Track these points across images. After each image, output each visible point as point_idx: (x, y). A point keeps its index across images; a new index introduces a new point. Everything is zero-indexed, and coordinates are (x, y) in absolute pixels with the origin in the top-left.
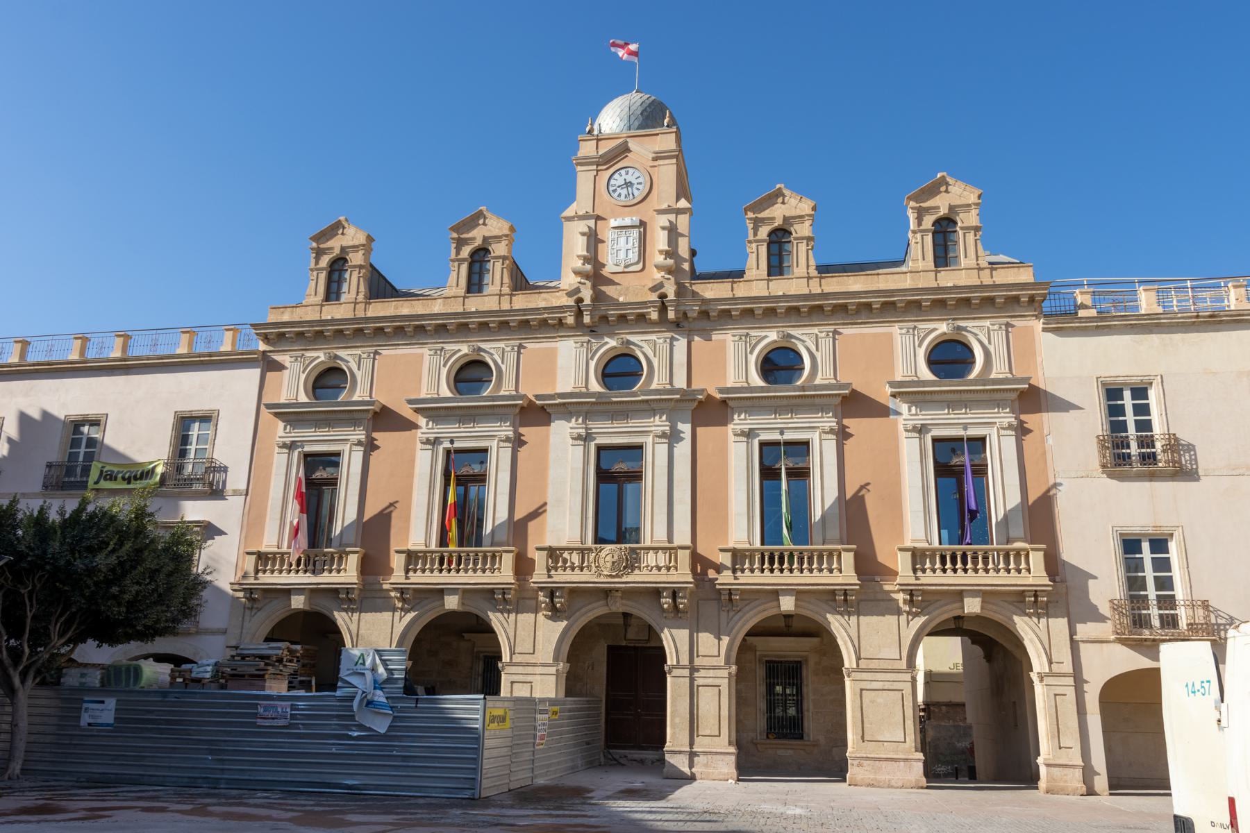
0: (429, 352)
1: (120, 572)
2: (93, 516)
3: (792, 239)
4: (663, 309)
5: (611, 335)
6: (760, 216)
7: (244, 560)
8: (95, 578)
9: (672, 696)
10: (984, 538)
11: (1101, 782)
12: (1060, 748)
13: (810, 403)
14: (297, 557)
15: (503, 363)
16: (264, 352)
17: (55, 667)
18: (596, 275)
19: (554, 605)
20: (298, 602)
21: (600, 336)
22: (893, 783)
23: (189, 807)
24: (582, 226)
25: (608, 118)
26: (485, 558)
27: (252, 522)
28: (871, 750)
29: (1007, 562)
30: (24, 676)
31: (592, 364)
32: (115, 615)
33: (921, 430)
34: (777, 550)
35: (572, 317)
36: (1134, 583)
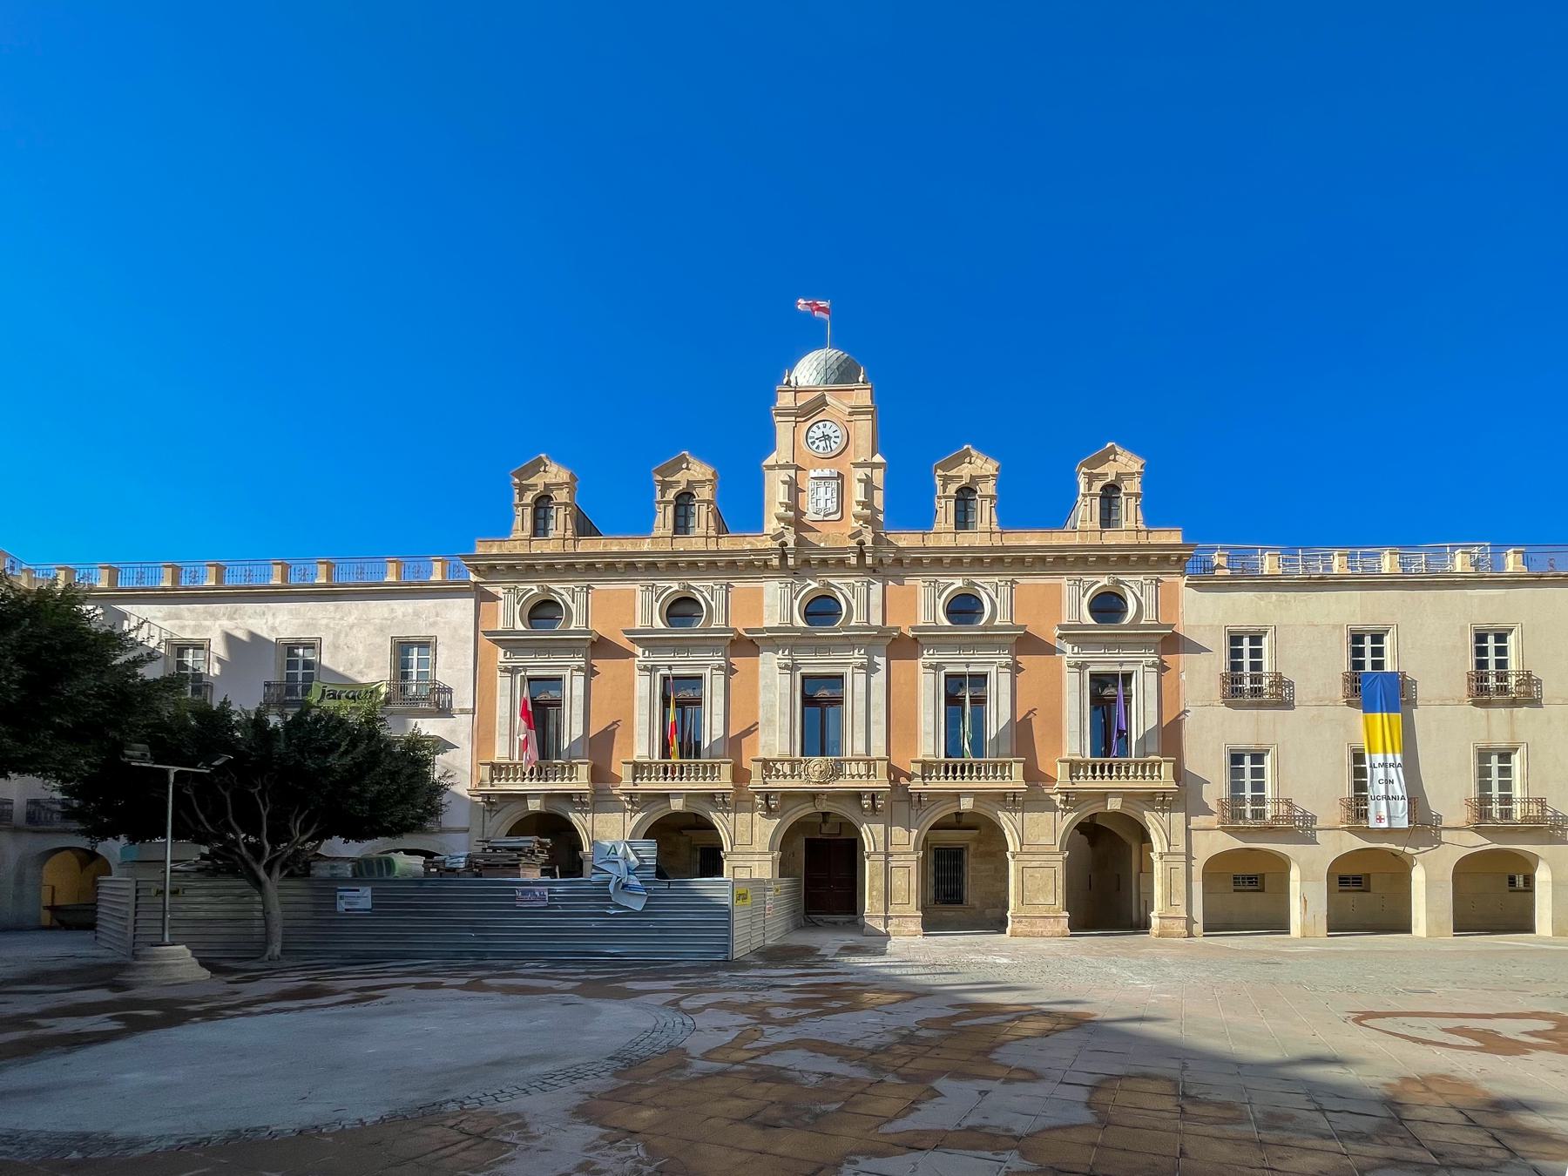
0: (640, 588)
1: (359, 772)
2: (318, 719)
3: (977, 497)
4: (861, 555)
5: (813, 578)
6: (948, 474)
7: (478, 771)
8: (331, 778)
9: (870, 875)
10: (1125, 751)
11: (1198, 928)
12: (1171, 905)
13: (989, 641)
14: (530, 767)
15: (712, 600)
16: (475, 583)
17: (301, 861)
18: (797, 521)
19: (769, 807)
20: (534, 805)
21: (803, 578)
22: (1044, 934)
23: (464, 981)
24: (784, 475)
25: (805, 371)
26: (705, 768)
27: (483, 736)
28: (1026, 911)
29: (1144, 770)
30: (269, 869)
31: (796, 603)
32: (359, 813)
33: (1081, 666)
34: (959, 762)
35: (778, 560)
36: (1236, 787)
